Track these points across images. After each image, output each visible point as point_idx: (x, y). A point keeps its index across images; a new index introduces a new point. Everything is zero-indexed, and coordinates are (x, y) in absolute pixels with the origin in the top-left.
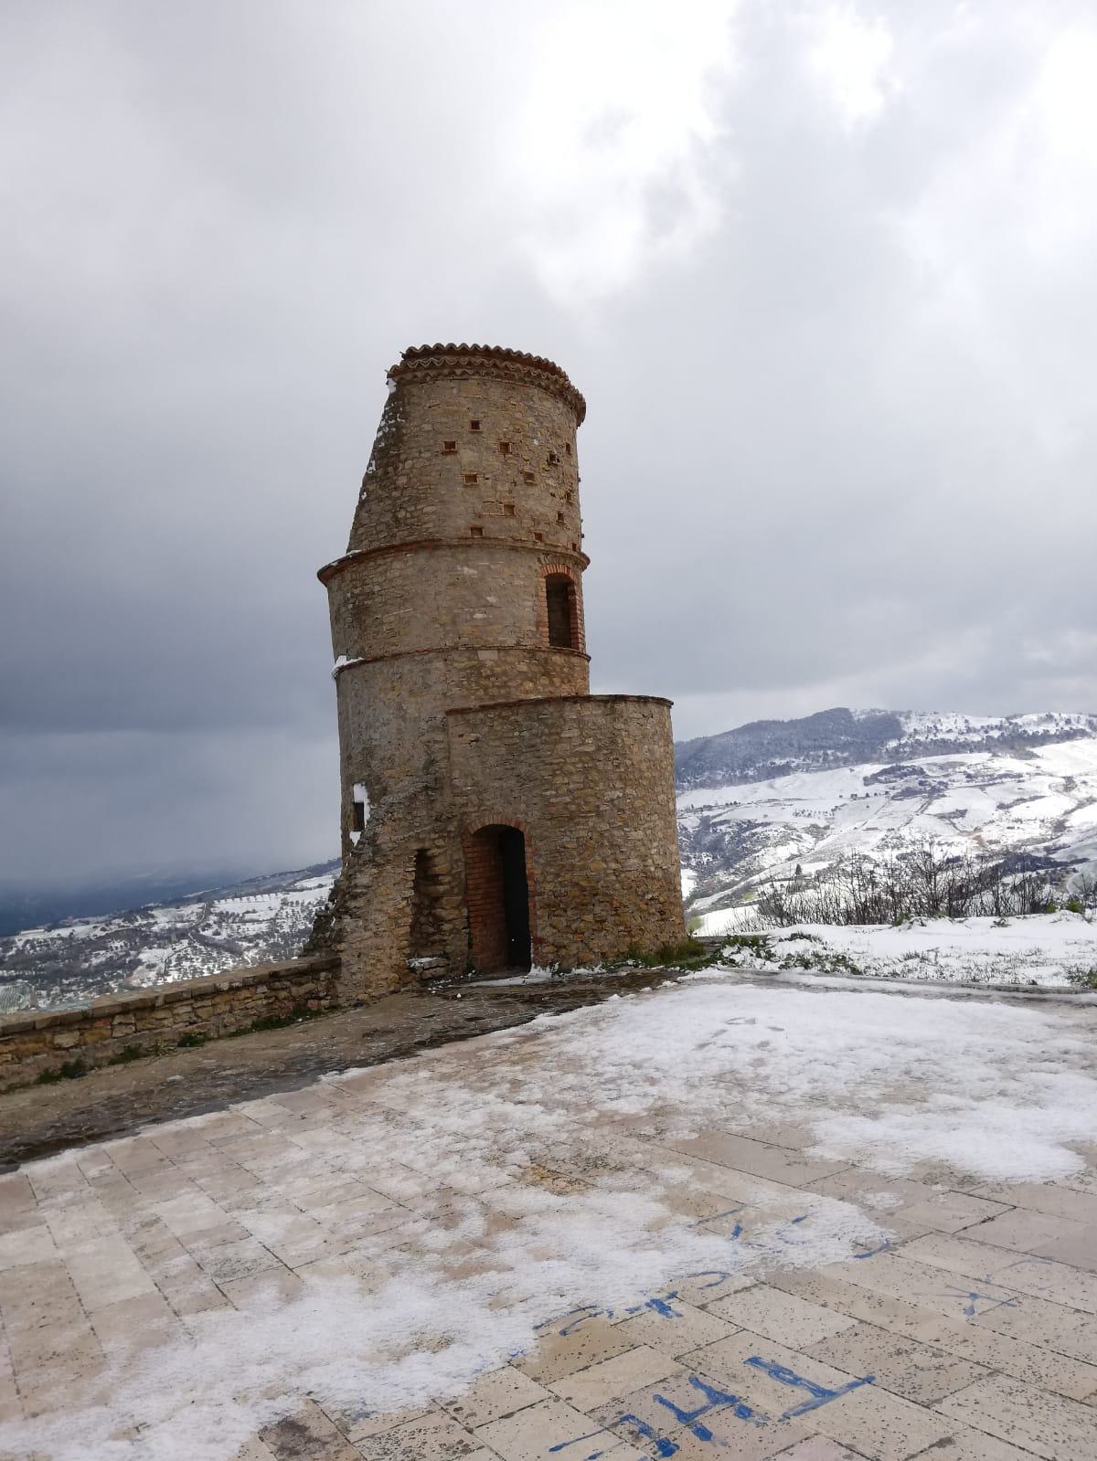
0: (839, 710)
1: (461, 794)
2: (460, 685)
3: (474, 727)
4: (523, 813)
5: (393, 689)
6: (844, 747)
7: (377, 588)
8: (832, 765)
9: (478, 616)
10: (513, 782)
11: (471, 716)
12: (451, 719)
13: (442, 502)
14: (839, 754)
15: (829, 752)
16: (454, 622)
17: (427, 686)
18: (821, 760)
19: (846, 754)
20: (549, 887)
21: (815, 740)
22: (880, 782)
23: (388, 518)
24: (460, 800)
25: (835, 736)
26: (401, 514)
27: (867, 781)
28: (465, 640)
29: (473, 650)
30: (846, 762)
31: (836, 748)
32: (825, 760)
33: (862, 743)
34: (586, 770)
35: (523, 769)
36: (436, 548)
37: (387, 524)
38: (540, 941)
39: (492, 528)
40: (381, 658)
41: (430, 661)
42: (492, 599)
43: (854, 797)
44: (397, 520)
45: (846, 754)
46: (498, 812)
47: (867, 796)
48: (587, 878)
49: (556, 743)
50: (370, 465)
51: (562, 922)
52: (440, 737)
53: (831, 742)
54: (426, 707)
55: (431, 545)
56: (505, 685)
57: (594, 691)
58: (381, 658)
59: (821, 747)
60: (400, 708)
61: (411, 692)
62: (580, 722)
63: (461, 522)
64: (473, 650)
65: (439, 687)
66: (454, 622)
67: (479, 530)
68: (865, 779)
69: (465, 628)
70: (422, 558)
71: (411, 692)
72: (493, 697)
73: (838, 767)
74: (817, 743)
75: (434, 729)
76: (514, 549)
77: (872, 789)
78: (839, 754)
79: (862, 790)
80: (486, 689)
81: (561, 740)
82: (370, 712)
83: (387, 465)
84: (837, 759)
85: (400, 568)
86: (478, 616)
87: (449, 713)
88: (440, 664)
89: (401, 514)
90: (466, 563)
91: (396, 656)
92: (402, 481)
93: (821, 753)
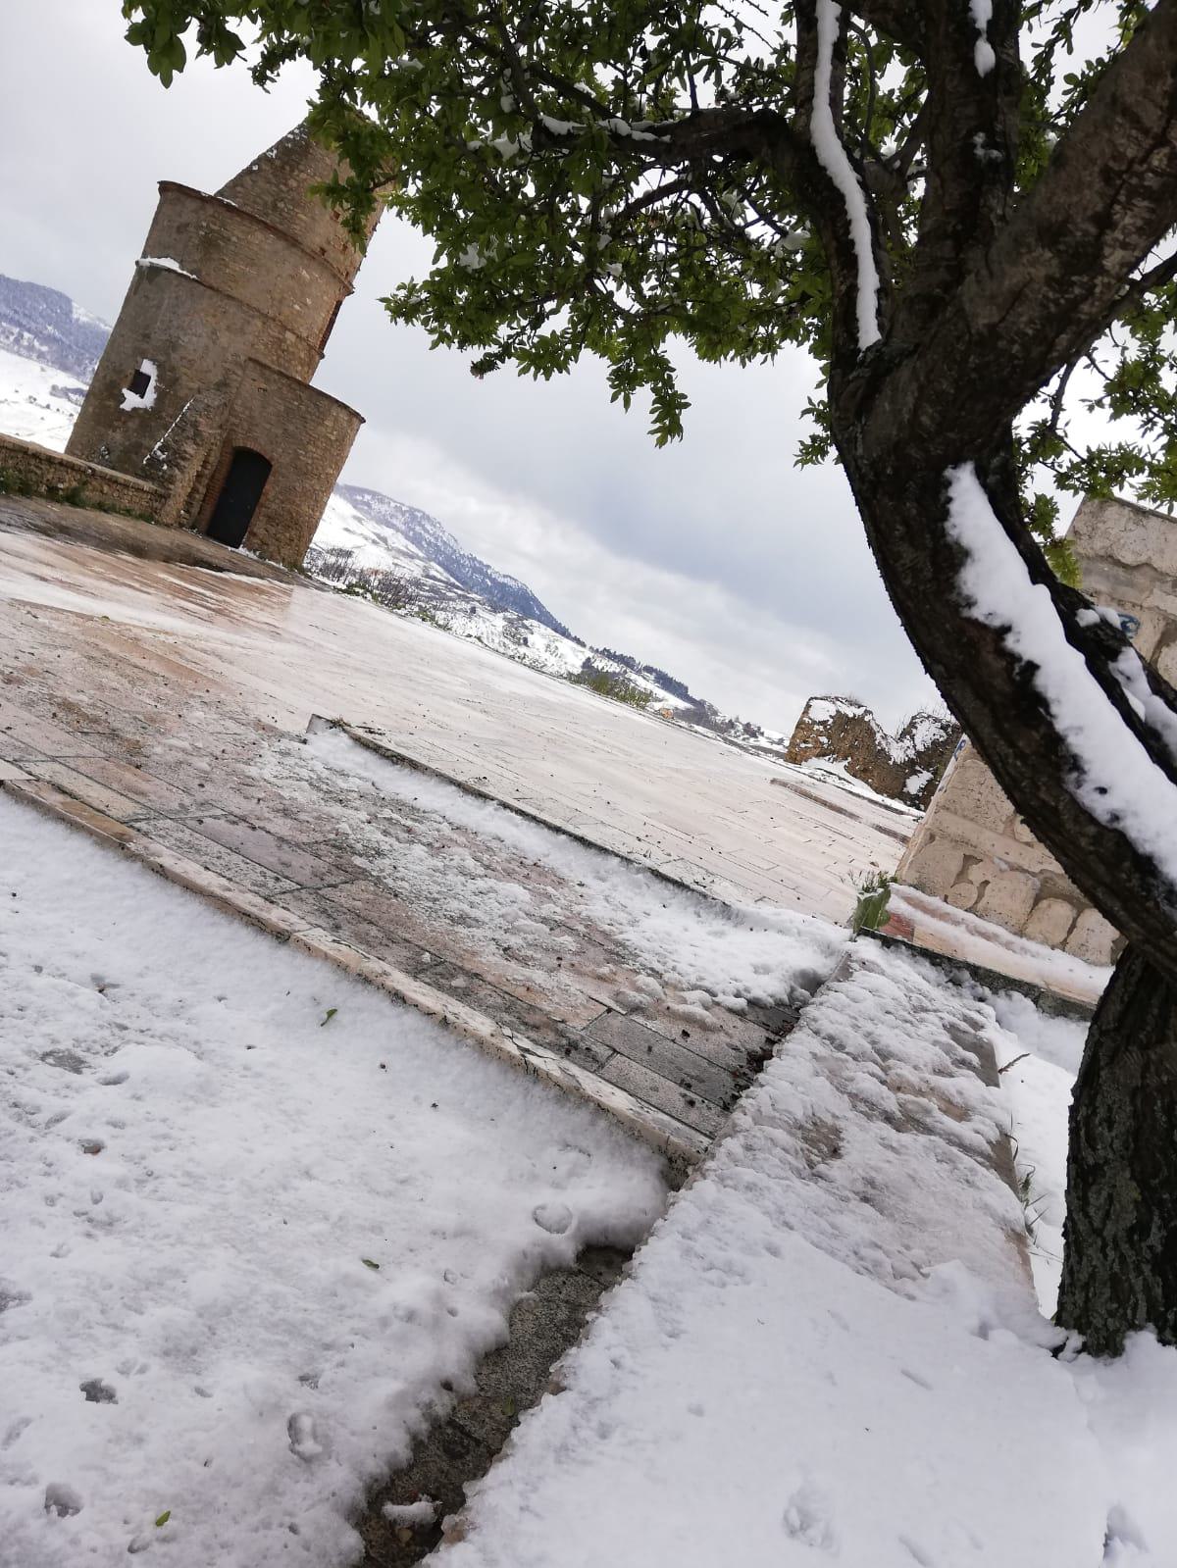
0: (61, 296)
1: (236, 417)
2: (266, 345)
3: (267, 381)
4: (279, 455)
5: (214, 316)
6: (48, 339)
7: (234, 239)
8: (23, 351)
9: (297, 307)
10: (280, 432)
11: (267, 372)
12: (251, 364)
13: (313, 218)
14: (36, 344)
15: (26, 335)
16: (280, 302)
17: (242, 331)
18: (12, 338)
19: (45, 349)
20: (274, 506)
21: (16, 312)
22: (69, 400)
23: (269, 199)
24: (233, 419)
25: (40, 320)
26: (281, 205)
27: (55, 391)
28: (282, 318)
29: (285, 328)
30: (41, 356)
31: (37, 334)
32: (17, 341)
33: (70, 347)
34: (325, 449)
35: (291, 428)
36: (294, 245)
37: (266, 203)
38: (255, 535)
39: (331, 255)
40: (217, 291)
41: (253, 317)
42: (309, 301)
43: (32, 400)
44: (275, 207)
45: (45, 349)
46: (259, 443)
47: (48, 407)
48: (298, 513)
49: (319, 424)
50: (271, 150)
51: (273, 530)
52: (240, 373)
53: (33, 325)
54: (236, 345)
55: (293, 242)
56: (289, 361)
57: (315, 383)
58: (217, 291)
59: (20, 325)
60: (214, 332)
61: (228, 328)
62: (336, 420)
63: (317, 240)
64: (285, 328)
65: (251, 338)
66: (280, 302)
67: (323, 251)
68: (54, 388)
69: (286, 311)
70: (280, 245)
71: (228, 328)
72: (279, 365)
73: (29, 357)
74: (17, 317)
75: (237, 364)
76: (334, 276)
77: (56, 402)
78: (36, 344)
79: (44, 398)
80: (279, 357)
81: (322, 424)
82: (187, 319)
83: (287, 163)
84: (31, 348)
85: (259, 238)
86: (297, 307)
87: (250, 359)
88: (259, 324)
89: (281, 205)
90: (306, 267)
91: (229, 297)
92: (293, 183)
93: (16, 330)
